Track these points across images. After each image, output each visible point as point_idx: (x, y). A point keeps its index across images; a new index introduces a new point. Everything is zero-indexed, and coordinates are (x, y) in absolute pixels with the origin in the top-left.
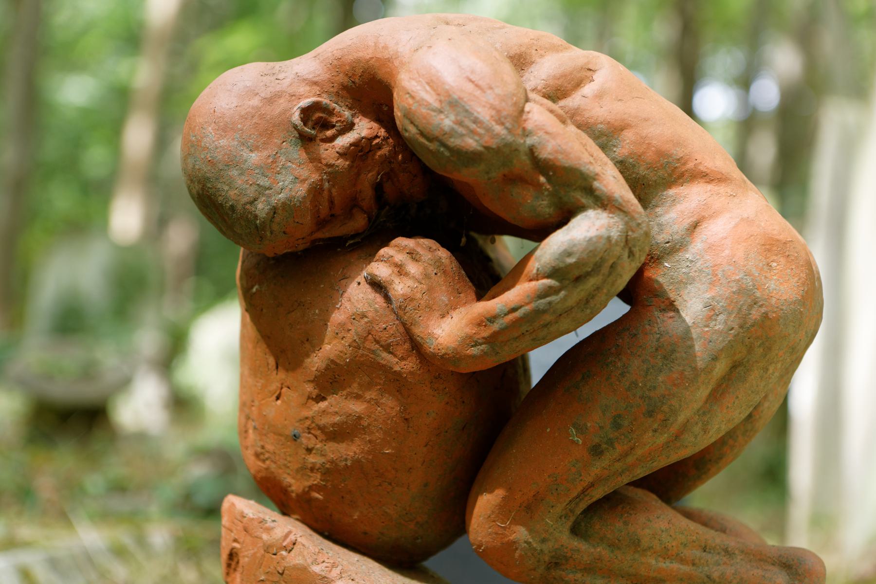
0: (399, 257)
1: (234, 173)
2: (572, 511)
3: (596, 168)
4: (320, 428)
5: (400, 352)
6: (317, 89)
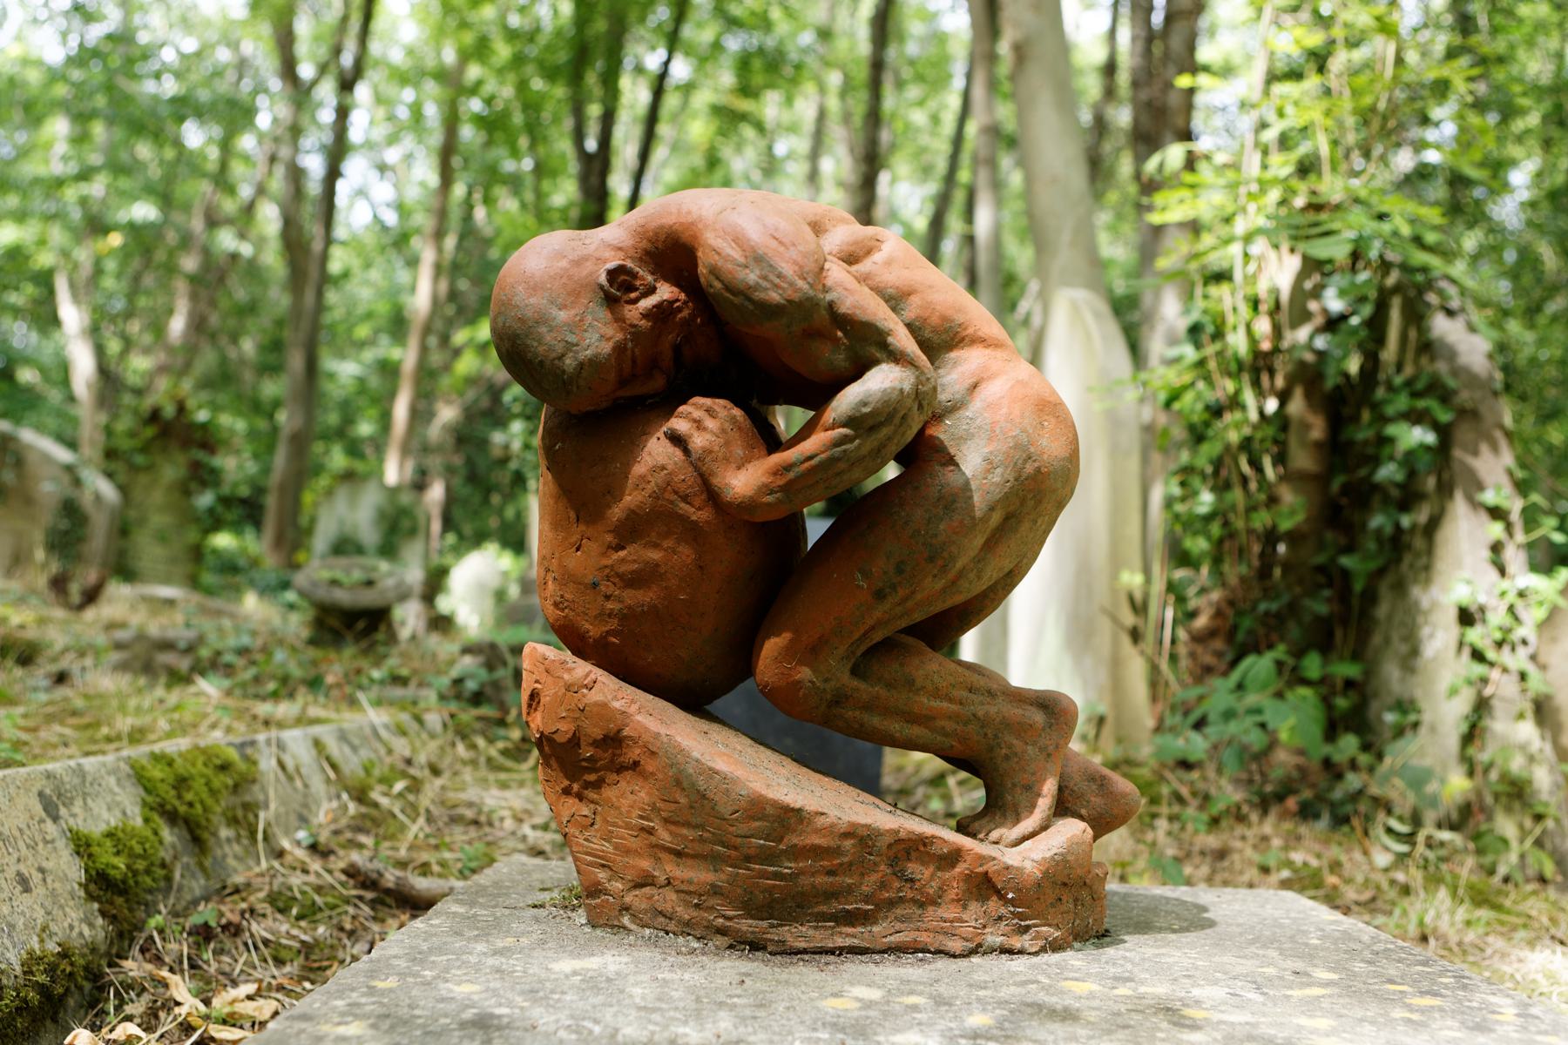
0: (697, 414)
1: (543, 329)
2: (853, 653)
3: (892, 326)
4: (617, 575)
5: (697, 502)
6: (621, 254)
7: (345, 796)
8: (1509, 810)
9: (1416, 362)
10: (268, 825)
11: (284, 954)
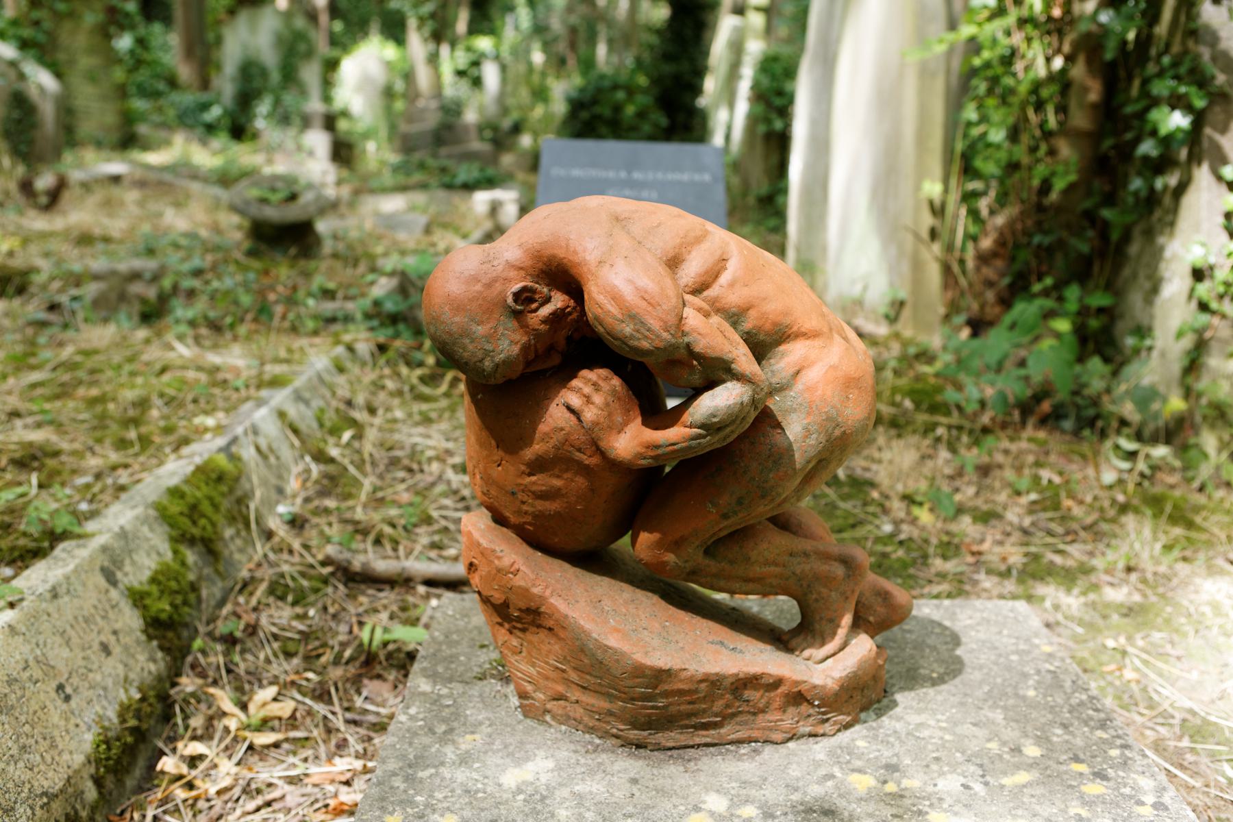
1: (467, 341)
7: (308, 459)
8: (1213, 427)
9: (1183, 43)
10: (257, 510)
11: (291, 647)
